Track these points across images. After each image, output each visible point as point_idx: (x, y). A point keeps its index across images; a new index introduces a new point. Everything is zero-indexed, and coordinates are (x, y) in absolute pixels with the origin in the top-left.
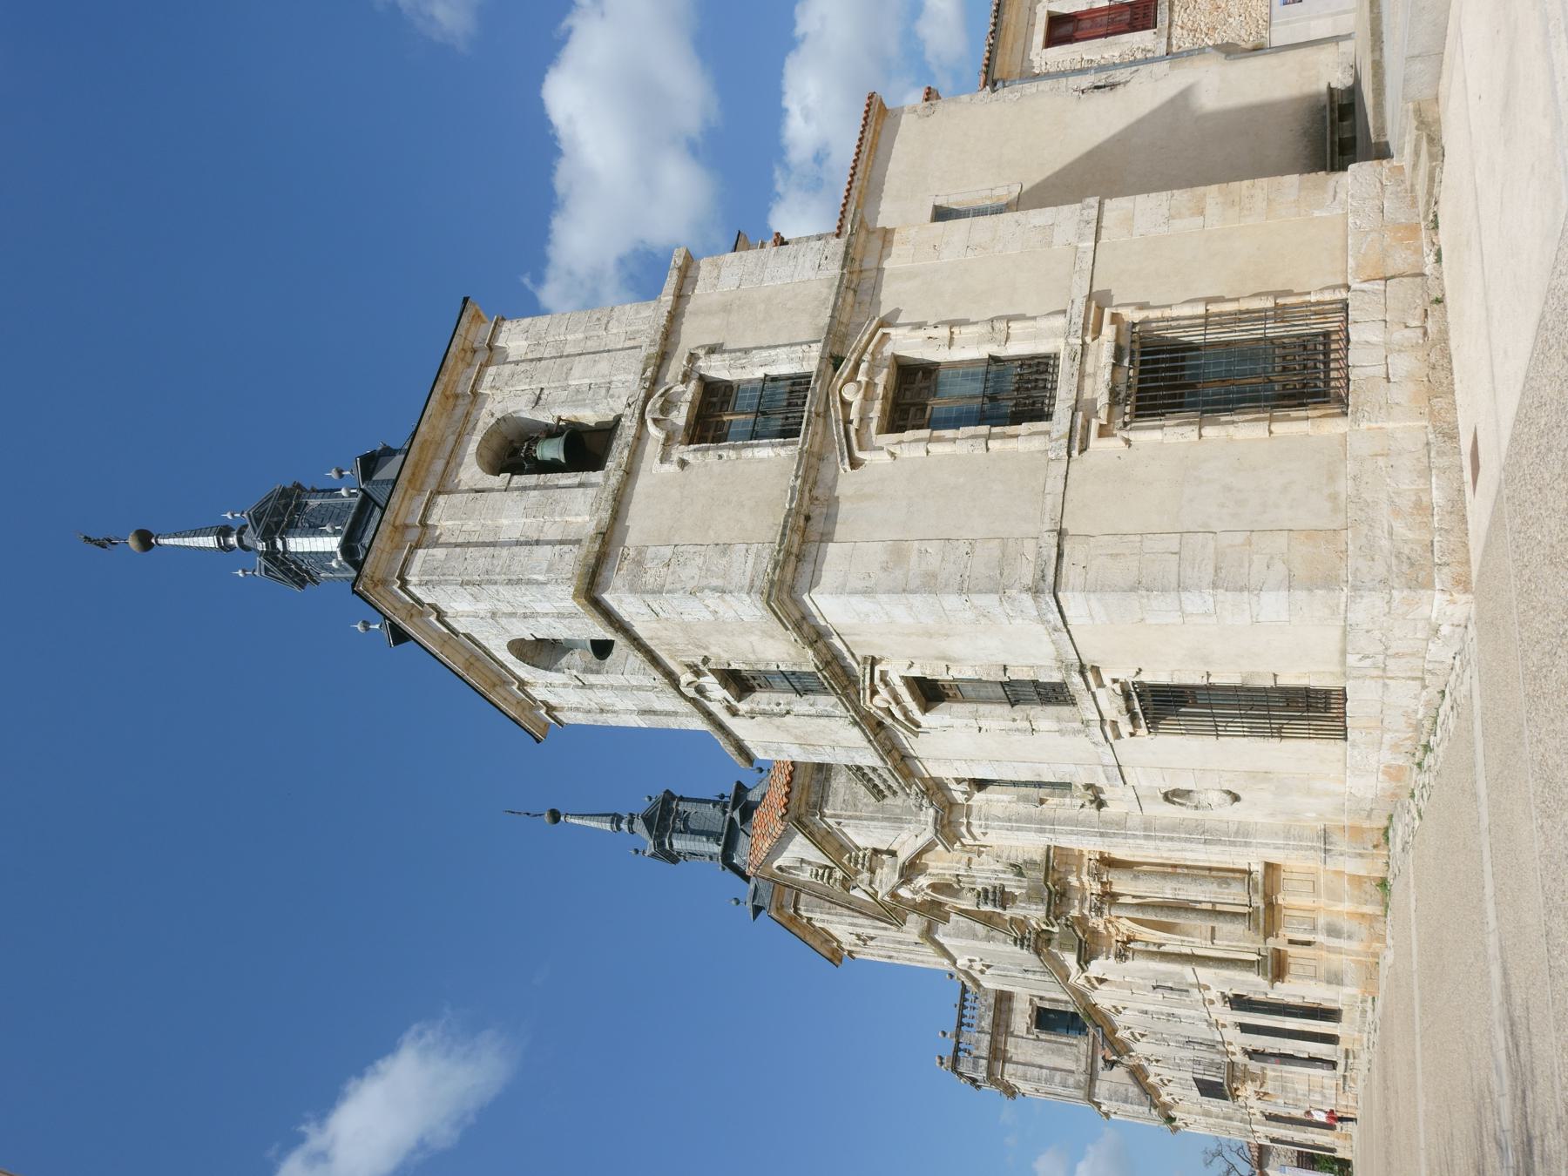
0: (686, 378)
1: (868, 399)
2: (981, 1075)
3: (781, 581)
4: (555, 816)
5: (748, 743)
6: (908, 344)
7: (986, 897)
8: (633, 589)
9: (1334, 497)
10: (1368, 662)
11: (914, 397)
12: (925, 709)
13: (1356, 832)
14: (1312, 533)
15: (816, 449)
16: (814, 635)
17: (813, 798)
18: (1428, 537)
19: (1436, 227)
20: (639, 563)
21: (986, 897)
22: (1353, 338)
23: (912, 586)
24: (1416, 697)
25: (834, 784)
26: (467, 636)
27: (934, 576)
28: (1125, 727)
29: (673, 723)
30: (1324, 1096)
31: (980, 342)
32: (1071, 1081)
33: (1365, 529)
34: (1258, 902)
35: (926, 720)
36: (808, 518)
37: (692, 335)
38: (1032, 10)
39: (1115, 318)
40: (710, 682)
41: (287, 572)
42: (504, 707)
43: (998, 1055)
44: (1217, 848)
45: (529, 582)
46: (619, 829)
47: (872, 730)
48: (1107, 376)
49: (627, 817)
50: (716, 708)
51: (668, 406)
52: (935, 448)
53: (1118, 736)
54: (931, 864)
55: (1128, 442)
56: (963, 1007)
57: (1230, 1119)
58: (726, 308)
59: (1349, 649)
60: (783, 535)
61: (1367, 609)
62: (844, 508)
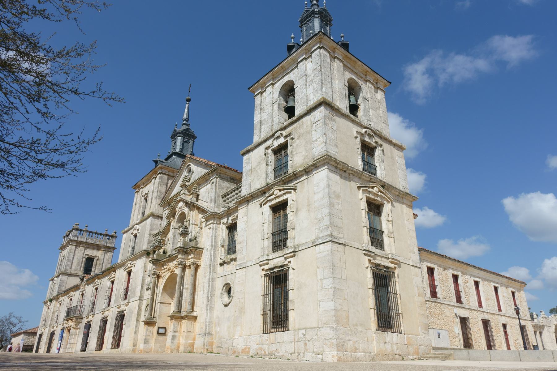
0: (376, 142)
1: (375, 194)
2: (71, 237)
3: (331, 160)
4: (189, 100)
5: (251, 154)
6: (387, 209)
7: (185, 228)
8: (325, 116)
9: (356, 325)
11: (375, 208)
12: (270, 207)
13: (211, 344)
14: (348, 317)
15: (363, 177)
16: (148, 217)
17: (222, 175)
18: (349, 351)
19: (420, 359)
20: (332, 119)
21: (185, 228)
22: (394, 334)
23: (331, 199)
24: (286, 352)
25: (226, 182)
27: (333, 206)
28: (266, 267)
30: (69, 348)
31: (388, 229)
32: (68, 268)
33: (350, 333)
34: (183, 314)
35: (267, 208)
36: (345, 171)
37: (386, 146)
38: (435, 263)
39: (395, 268)
40: (282, 140)
41: (307, 17)
42: (265, 78)
43: (78, 244)
44: (205, 301)
45: (322, 86)
46: (184, 121)
47: (263, 190)
48: (382, 264)
49: (189, 123)
50: (269, 143)
51: (369, 135)
52: (363, 212)
53: (261, 266)
54: (194, 213)
55: (367, 268)
56: (96, 233)
57: (51, 320)
60: (343, 163)
61: (327, 332)
62: (348, 183)
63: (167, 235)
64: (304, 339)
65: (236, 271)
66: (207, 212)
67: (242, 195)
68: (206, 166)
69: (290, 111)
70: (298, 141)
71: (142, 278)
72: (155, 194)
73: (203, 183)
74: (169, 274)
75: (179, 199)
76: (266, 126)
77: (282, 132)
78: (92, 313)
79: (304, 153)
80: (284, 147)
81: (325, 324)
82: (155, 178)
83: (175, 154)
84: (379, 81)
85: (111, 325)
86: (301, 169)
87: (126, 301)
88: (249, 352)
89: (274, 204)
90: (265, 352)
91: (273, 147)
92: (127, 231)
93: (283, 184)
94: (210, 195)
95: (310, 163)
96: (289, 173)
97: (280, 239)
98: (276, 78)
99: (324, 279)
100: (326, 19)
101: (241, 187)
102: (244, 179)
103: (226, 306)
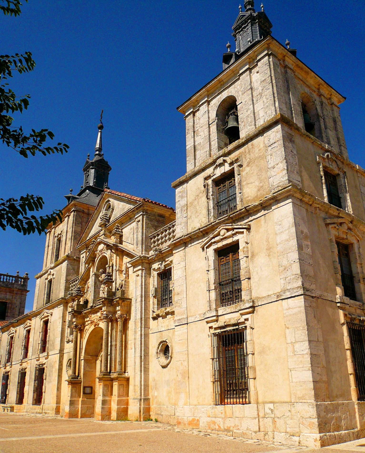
4: (101, 128)
5: (185, 185)
12: (215, 250)
21: (109, 276)
26: (239, 79)
28: (215, 325)
35: (211, 251)
40: (227, 168)
47: (205, 230)
50: (209, 171)
53: (207, 322)
55: (343, 324)
59: (275, 405)
63: (86, 282)
65: (174, 327)
66: (134, 257)
68: (129, 202)
69: (232, 134)
70: (248, 169)
71: (60, 329)
72: (69, 235)
74: (93, 327)
76: (202, 151)
77: (225, 158)
78: (9, 364)
79: (257, 183)
80: (229, 176)
82: (69, 216)
83: (89, 188)
84: (333, 96)
85: (30, 378)
86: (257, 204)
87: (45, 354)
88: (199, 425)
89: (221, 247)
90: (219, 426)
91: (214, 177)
92: (41, 276)
93: (231, 223)
94: (135, 236)
95: (270, 196)
96: (238, 209)
97: (229, 289)
98: (211, 95)
99: (296, 342)
101: (174, 226)
103: (164, 367)
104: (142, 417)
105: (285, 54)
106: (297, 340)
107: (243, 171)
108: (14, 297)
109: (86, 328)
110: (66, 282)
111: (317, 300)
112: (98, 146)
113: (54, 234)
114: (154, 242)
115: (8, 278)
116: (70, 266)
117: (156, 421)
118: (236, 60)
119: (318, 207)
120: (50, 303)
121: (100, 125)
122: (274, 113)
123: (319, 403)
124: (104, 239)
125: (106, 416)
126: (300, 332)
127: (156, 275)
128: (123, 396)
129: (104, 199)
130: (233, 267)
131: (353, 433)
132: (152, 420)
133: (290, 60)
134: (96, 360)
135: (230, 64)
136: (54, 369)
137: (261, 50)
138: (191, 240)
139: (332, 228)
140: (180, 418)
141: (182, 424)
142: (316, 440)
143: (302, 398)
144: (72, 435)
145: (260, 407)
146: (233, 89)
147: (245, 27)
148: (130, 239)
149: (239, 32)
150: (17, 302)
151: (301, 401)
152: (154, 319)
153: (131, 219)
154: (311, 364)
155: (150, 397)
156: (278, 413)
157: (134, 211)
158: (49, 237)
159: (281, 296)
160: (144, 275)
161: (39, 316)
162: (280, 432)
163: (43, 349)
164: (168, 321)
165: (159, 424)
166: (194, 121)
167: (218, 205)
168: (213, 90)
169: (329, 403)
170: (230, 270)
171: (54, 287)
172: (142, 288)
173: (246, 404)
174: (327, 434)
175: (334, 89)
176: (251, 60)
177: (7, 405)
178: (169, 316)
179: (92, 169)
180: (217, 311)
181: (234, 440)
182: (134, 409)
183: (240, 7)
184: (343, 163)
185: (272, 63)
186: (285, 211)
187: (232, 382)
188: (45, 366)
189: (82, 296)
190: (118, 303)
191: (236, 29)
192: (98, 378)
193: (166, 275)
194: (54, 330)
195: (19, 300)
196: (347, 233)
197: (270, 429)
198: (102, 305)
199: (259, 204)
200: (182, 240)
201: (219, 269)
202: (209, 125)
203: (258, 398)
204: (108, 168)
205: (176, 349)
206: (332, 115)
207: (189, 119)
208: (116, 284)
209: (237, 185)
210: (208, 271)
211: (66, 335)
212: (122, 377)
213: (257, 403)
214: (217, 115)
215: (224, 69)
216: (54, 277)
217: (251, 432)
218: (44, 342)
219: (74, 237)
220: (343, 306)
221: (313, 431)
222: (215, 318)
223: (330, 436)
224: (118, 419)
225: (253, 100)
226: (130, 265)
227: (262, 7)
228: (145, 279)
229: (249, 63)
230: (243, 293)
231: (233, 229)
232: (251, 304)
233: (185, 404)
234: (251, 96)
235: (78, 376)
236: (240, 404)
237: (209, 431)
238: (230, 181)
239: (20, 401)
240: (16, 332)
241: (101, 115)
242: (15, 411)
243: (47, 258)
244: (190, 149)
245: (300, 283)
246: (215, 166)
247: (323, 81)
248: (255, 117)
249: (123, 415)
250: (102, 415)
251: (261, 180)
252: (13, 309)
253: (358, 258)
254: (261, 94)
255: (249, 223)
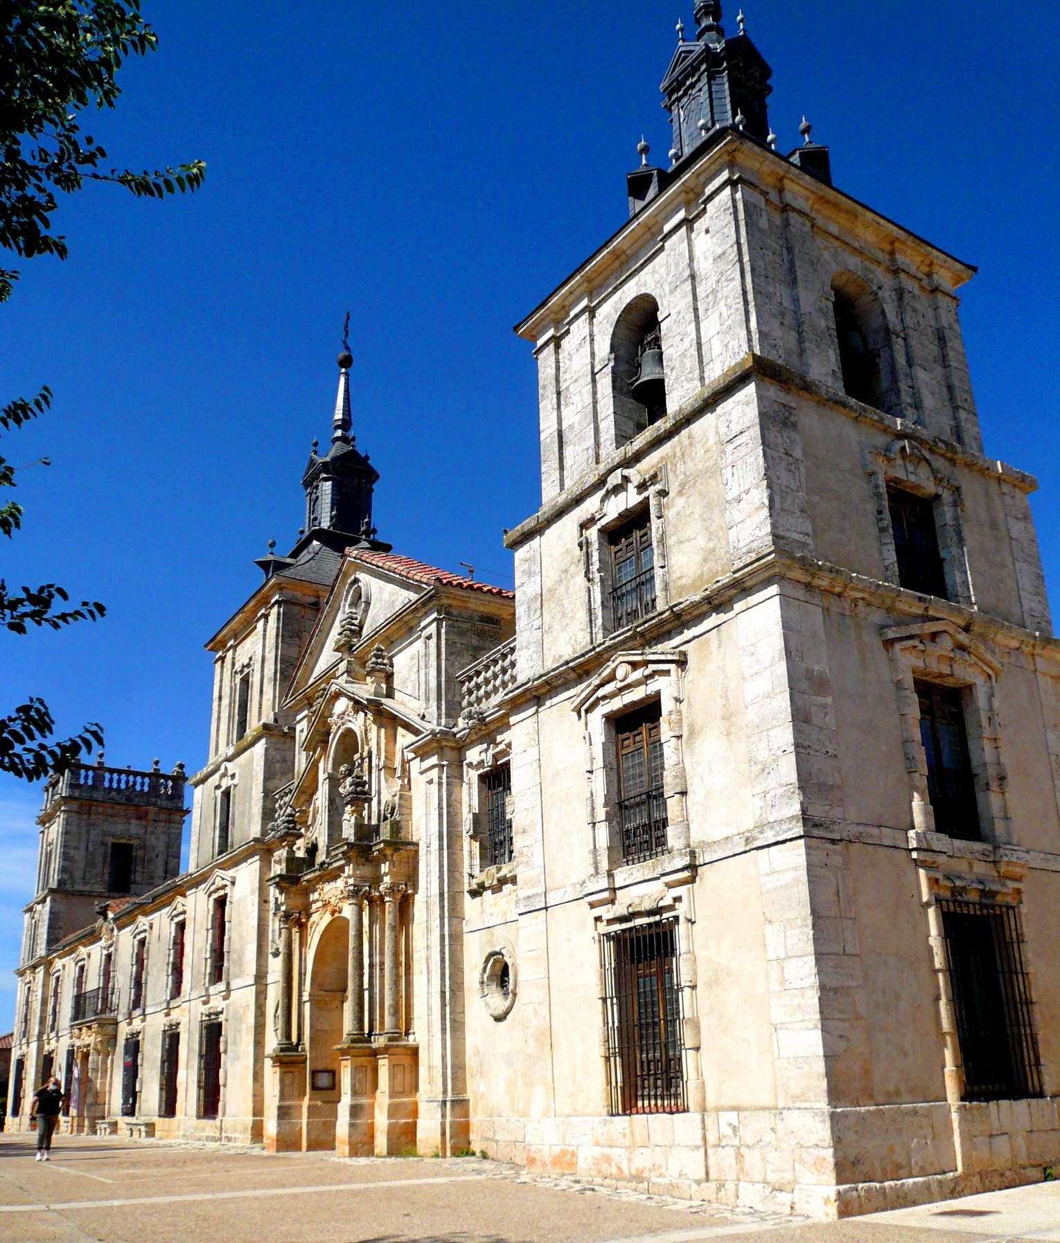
4: (346, 362)
5: (535, 543)
7: (357, 785)
10: (729, 1132)
26: (662, 249)
28: (607, 912)
29: (549, 467)
35: (596, 720)
40: (631, 498)
46: (337, 427)
47: (581, 664)
50: (591, 505)
53: (592, 906)
55: (928, 905)
58: (994, 525)
59: (743, 1114)
64: (736, 1142)
65: (517, 917)
67: (521, 679)
73: (402, 638)
74: (327, 918)
75: (333, 688)
77: (626, 472)
78: (138, 1012)
79: (701, 541)
80: (637, 519)
81: (796, 1098)
82: (266, 616)
83: (319, 534)
84: (936, 269)
86: (697, 598)
87: (221, 986)
90: (620, 1169)
91: (603, 522)
92: (203, 780)
95: (725, 579)
97: (637, 820)
98: (598, 289)
99: (788, 957)
100: (747, 74)
101: (513, 650)
102: (520, 624)
103: (498, 1019)
104: (448, 1146)
105: (781, 173)
106: (790, 954)
107: (668, 507)
108: (150, 829)
109: (312, 920)
110: (266, 797)
111: (847, 848)
112: (339, 415)
113: (233, 664)
114: (470, 692)
115: (131, 778)
116: (272, 752)
117: (485, 1156)
118: (663, 188)
119: (863, 599)
120: (228, 852)
121: (342, 354)
122: (745, 348)
123: (839, 1110)
124: (348, 686)
125: (362, 1145)
126: (796, 932)
127: (475, 781)
128: (402, 1093)
129: (346, 576)
130: (649, 761)
131: (940, 1182)
132: (473, 1154)
133: (800, 190)
134: (343, 1002)
135: (648, 199)
136: (244, 1026)
137: (714, 168)
138: (549, 691)
139: (902, 650)
140: (533, 1148)
141: (539, 1163)
142: (827, 1202)
143: (801, 1097)
144: (259, 1193)
145: (709, 1121)
146: (650, 276)
147: (693, 86)
148: (410, 685)
149: (679, 99)
150: (157, 842)
151: (798, 1105)
152: (475, 894)
153: (411, 630)
154: (821, 1012)
155: (469, 1095)
156: (748, 1136)
157: (416, 609)
158: (222, 672)
159: (755, 839)
160: (444, 780)
161: (203, 886)
162: (752, 1182)
163: (217, 974)
164: (505, 900)
165: (487, 1165)
166: (557, 362)
167: (613, 595)
168: (601, 278)
169: (872, 1108)
170: (645, 769)
171: (236, 809)
172: (440, 815)
173: (678, 1111)
174: (861, 1185)
175: (937, 249)
176: (692, 195)
177: (139, 1119)
178: (508, 888)
179: (326, 480)
180: (610, 875)
181: (649, 1203)
182: (429, 1127)
183: (678, 26)
184: (953, 462)
185: (741, 206)
186: (761, 621)
187: (648, 1059)
188: (222, 1018)
189: (300, 836)
190: (385, 856)
191: (670, 91)
192: (272, 1058)
193: (497, 779)
194: (240, 923)
195: (163, 838)
196: (952, 659)
197: (731, 1175)
198: (343, 862)
199: (704, 599)
200: (528, 690)
201: (615, 769)
202: (594, 374)
203: (704, 1099)
204: (372, 476)
205: (525, 973)
206: (933, 323)
207: (545, 359)
208: (379, 803)
209: (655, 544)
210: (591, 772)
211: (270, 938)
212: (398, 1046)
213: (704, 1110)
214: (613, 348)
215: (632, 214)
216: (236, 781)
217: (688, 1182)
218: (218, 955)
219: (282, 673)
220: (924, 856)
221: (824, 1178)
222: (606, 895)
223: (869, 1190)
224: (390, 1153)
225: (696, 310)
226: (412, 755)
227: (741, 21)
228: (448, 790)
229: (688, 204)
230: (670, 831)
231: (647, 663)
232: (686, 861)
233: (545, 1114)
234: (690, 298)
235: (298, 1044)
236: (664, 1112)
237: (598, 1180)
238: (643, 532)
239: (169, 1108)
240: (151, 928)
241: (346, 326)
242: (157, 1134)
243: (218, 730)
244: (548, 440)
245: (796, 809)
246: (603, 492)
247: (901, 232)
248: (700, 356)
249: (404, 1140)
250: (350, 1143)
251: (711, 533)
252: (150, 861)
253: (985, 723)
254: (714, 292)
255: (682, 648)
